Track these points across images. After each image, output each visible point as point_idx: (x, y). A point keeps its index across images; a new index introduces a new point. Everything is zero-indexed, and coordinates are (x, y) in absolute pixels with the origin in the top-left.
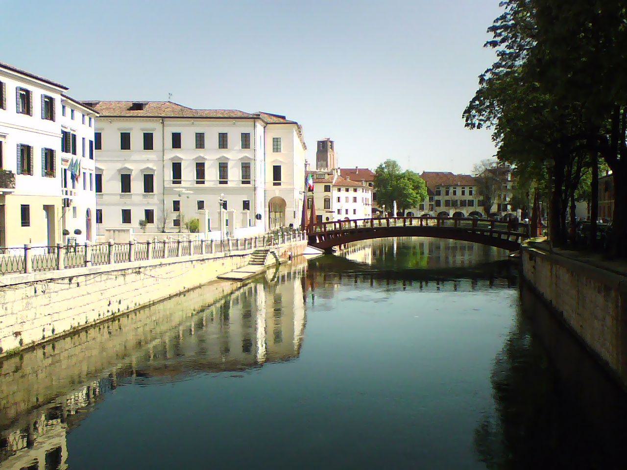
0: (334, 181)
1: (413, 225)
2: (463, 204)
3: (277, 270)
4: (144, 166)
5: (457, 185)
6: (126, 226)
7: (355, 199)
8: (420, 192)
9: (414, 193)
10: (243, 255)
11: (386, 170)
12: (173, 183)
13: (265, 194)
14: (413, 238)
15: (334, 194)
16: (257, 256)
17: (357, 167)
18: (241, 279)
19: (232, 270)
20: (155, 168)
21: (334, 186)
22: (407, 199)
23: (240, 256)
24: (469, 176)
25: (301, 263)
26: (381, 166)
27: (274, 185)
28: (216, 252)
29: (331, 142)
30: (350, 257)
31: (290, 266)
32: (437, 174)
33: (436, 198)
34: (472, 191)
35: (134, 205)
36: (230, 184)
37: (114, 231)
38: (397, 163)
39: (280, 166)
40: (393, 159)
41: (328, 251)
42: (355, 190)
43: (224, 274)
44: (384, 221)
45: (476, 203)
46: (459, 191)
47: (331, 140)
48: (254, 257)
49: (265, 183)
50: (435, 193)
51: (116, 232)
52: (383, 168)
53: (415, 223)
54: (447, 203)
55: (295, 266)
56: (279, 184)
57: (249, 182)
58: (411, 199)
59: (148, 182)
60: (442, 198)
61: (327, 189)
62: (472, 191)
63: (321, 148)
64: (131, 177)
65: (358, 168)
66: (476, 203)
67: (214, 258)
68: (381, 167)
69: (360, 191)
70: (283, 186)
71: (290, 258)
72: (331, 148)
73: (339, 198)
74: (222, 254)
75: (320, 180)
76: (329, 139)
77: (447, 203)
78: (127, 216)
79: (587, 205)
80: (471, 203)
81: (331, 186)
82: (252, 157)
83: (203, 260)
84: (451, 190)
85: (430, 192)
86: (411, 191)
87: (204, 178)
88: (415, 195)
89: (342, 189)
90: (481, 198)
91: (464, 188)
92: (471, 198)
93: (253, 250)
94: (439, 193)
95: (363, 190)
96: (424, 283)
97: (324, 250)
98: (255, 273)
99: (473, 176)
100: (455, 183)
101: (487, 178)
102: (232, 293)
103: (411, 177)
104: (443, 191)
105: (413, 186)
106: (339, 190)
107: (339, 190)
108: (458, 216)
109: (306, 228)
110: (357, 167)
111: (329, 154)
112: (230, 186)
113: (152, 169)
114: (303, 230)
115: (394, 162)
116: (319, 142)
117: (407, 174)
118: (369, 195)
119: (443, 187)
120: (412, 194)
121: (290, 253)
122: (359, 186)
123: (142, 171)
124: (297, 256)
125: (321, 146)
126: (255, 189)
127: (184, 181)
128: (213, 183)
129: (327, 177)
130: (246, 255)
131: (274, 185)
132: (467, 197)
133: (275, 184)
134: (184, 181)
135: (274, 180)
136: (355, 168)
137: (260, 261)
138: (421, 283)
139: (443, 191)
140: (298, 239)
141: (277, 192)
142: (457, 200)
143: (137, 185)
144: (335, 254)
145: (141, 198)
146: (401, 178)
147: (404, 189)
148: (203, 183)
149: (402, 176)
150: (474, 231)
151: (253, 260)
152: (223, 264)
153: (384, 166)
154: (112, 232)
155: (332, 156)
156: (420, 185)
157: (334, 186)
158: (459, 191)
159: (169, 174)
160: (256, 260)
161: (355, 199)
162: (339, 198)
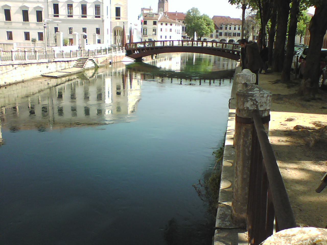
0: (159, 19)
1: (208, 46)
2: (234, 35)
3: (96, 71)
4: (36, 5)
5: (232, 24)
6: (10, 42)
7: (171, 30)
9: (207, 28)
10: (68, 61)
11: (191, 14)
12: (54, 17)
13: (111, 24)
14: (204, 54)
15: (159, 26)
16: (80, 62)
17: (176, 11)
18: (57, 77)
19: (57, 71)
20: (43, 7)
22: (203, 31)
23: (64, 61)
25: (120, 67)
26: (189, 11)
27: (116, 19)
28: (39, 59)
30: (158, 65)
31: (112, 68)
32: (222, 17)
33: (220, 31)
34: (236, 27)
35: (31, 29)
36: (74, 18)
37: (4, 44)
38: (198, 10)
39: (120, 8)
41: (139, 59)
42: (171, 25)
43: (49, 73)
44: (214, 44)
46: (233, 27)
48: (78, 62)
49: (111, 18)
50: (219, 28)
51: (5, 45)
52: (190, 13)
53: (210, 45)
54: (226, 34)
55: (116, 68)
57: (99, 17)
58: (205, 31)
59: (39, 15)
60: (223, 31)
61: (155, 23)
62: (236, 27)
64: (29, 12)
65: (177, 12)
67: (37, 63)
68: (189, 12)
69: (174, 25)
70: (121, 20)
71: (110, 63)
73: (161, 29)
74: (46, 61)
75: (151, 18)
77: (226, 34)
78: (27, 36)
79: (300, 38)
83: (25, 64)
84: (228, 27)
85: (216, 27)
86: (205, 26)
87: (58, 13)
88: (207, 29)
89: (163, 24)
91: (236, 26)
93: (78, 58)
94: (221, 28)
95: (176, 24)
96: (212, 81)
97: (135, 59)
98: (70, 73)
100: (231, 23)
102: (57, 85)
104: (224, 27)
105: (207, 23)
106: (162, 24)
107: (162, 24)
108: (231, 41)
109: (124, 45)
110: (176, 11)
112: (60, 18)
113: (41, 8)
114: (123, 46)
115: (197, 9)
117: (203, 17)
118: (180, 28)
119: (224, 24)
121: (110, 61)
122: (173, 22)
123: (35, 8)
124: (117, 62)
126: (103, 21)
127: (61, 15)
128: (78, 17)
129: (155, 16)
130: (71, 61)
131: (116, 19)
132: (237, 31)
133: (117, 19)
134: (61, 15)
135: (116, 16)
136: (175, 12)
137: (81, 65)
138: (220, 80)
140: (117, 52)
141: (118, 23)
142: (231, 33)
143: (33, 17)
144: (143, 62)
145: (21, 24)
147: (201, 25)
148: (86, 17)
149: (201, 18)
150: (234, 52)
151: (76, 64)
152: (47, 67)
153: (191, 11)
154: (3, 44)
155: (167, 5)
156: (210, 23)
158: (233, 27)
159: (51, 10)
160: (78, 64)
161: (171, 30)
162: (161, 29)
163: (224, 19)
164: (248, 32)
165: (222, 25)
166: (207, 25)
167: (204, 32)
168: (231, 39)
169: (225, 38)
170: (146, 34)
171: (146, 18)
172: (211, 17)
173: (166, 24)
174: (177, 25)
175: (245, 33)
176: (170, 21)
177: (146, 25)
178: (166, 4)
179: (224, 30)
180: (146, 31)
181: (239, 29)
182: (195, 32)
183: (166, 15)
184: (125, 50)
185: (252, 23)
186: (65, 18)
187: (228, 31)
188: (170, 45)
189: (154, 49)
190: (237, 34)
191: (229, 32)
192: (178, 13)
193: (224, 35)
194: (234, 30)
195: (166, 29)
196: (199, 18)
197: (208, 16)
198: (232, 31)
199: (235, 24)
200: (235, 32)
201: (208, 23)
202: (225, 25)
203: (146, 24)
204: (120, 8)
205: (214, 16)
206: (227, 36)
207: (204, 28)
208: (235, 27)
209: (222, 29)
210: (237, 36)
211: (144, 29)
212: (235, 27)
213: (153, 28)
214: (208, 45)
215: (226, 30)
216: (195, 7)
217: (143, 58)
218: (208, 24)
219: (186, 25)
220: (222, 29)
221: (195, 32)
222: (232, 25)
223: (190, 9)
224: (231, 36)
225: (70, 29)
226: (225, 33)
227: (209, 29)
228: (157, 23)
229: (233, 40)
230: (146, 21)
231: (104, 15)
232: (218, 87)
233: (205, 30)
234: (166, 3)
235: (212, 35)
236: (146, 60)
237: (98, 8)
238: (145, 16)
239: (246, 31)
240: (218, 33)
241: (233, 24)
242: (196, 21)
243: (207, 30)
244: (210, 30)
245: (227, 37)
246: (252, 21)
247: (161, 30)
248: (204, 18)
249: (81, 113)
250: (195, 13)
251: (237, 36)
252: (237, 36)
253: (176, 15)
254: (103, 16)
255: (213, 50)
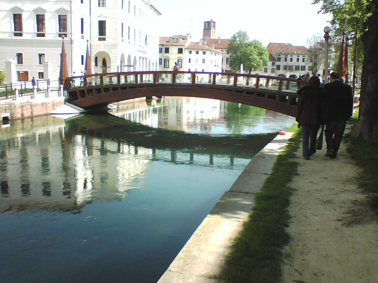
2: (297, 68)
5: (294, 54)
7: (204, 61)
8: (263, 57)
9: (258, 58)
11: (238, 39)
15: (186, 55)
21: (186, 48)
22: (252, 63)
24: (303, 47)
26: (234, 35)
29: (214, 22)
32: (280, 44)
33: (277, 63)
38: (247, 33)
39: (105, 21)
40: (243, 30)
44: (263, 81)
45: (307, 68)
46: (295, 58)
47: (214, 21)
52: (235, 38)
54: (285, 68)
56: (104, 39)
58: (255, 63)
60: (282, 63)
61: (180, 51)
63: (207, 27)
66: (307, 68)
68: (234, 37)
69: (208, 53)
72: (214, 27)
73: (190, 59)
75: (175, 44)
76: (212, 20)
77: (285, 68)
80: (303, 68)
81: (184, 49)
82: (68, 9)
84: (289, 58)
85: (271, 58)
86: (255, 56)
88: (258, 60)
90: (311, 64)
92: (303, 64)
94: (279, 60)
97: (82, 109)
99: (308, 47)
100: (293, 52)
101: (316, 49)
103: (257, 45)
104: (283, 57)
105: (258, 53)
106: (190, 52)
109: (64, 82)
111: (211, 31)
116: (205, 23)
118: (219, 58)
119: (283, 54)
120: (256, 59)
125: (207, 25)
127: (176, 59)
132: (301, 63)
133: (100, 39)
134: (176, 59)
135: (99, 35)
136: (218, 38)
139: (283, 58)
141: (98, 47)
146: (249, 46)
147: (250, 55)
149: (250, 45)
153: (236, 35)
156: (263, 52)
157: (186, 48)
158: (295, 58)
161: (204, 61)
162: (190, 59)
163: (283, 47)
164: (316, 64)
165: (280, 56)
166: (258, 54)
167: (254, 64)
168: (292, 73)
169: (284, 73)
170: (168, 66)
171: (168, 44)
172: (265, 45)
173: (197, 53)
174: (214, 54)
175: (312, 66)
176: (202, 48)
177: (168, 54)
178: (213, 31)
179: (283, 62)
180: (181, 62)
181: (303, 61)
182: (242, 65)
183: (206, 43)
184: (66, 92)
185: (321, 51)
186: (10, 38)
187: (289, 63)
188: (210, 81)
189: (128, 88)
190: (300, 67)
191: (289, 65)
192: (222, 40)
193: (283, 69)
194: (297, 61)
195: (197, 60)
196: (248, 45)
197: (261, 43)
198: (294, 63)
199: (298, 53)
200: (298, 64)
201: (260, 51)
202: (284, 56)
203: (168, 53)
204: (105, 21)
205: (270, 43)
206: (287, 70)
207: (253, 58)
208: (298, 57)
209: (280, 61)
210: (301, 70)
211: (165, 60)
212: (298, 57)
213: (178, 58)
214: (144, 79)
215: (286, 62)
216: (243, 30)
217: (110, 106)
218: (261, 54)
219: (230, 54)
220: (280, 61)
221: (242, 65)
222: (293, 55)
223: (236, 33)
224: (292, 70)
225: (41, 56)
226: (284, 65)
227: (261, 61)
228: (183, 51)
229: (295, 75)
230: (169, 48)
231: (72, 33)
232: (226, 171)
233: (256, 62)
234: (212, 30)
235: (267, 68)
236: (118, 110)
237: (63, 22)
238: (168, 42)
239: (313, 63)
240: (274, 66)
241: (295, 53)
242: (243, 50)
243: (258, 62)
244: (263, 61)
245: (287, 72)
246: (321, 49)
247: (190, 61)
248: (255, 45)
249: (36, 192)
250: (242, 39)
251: (300, 69)
252: (300, 69)
253: (219, 42)
254: (71, 34)
255: (236, 91)
